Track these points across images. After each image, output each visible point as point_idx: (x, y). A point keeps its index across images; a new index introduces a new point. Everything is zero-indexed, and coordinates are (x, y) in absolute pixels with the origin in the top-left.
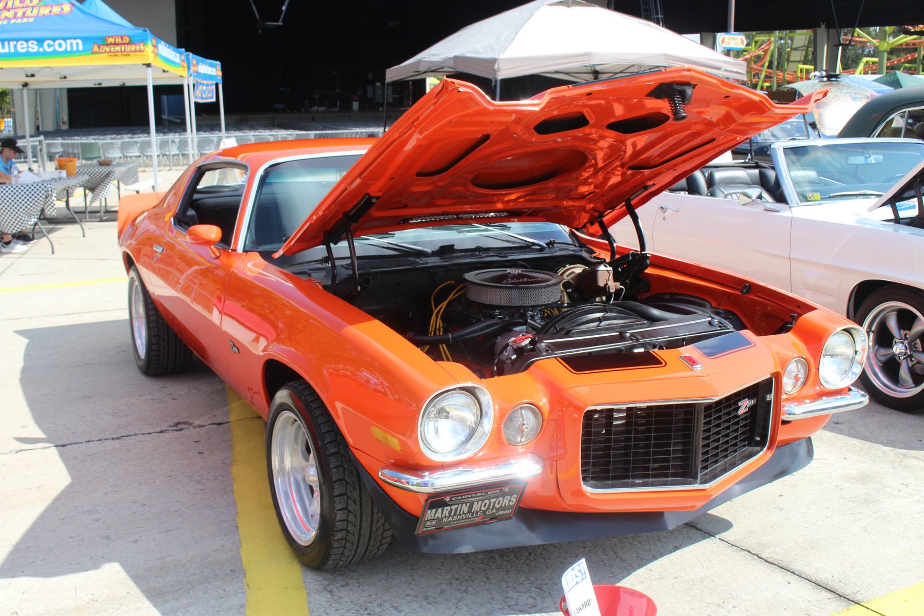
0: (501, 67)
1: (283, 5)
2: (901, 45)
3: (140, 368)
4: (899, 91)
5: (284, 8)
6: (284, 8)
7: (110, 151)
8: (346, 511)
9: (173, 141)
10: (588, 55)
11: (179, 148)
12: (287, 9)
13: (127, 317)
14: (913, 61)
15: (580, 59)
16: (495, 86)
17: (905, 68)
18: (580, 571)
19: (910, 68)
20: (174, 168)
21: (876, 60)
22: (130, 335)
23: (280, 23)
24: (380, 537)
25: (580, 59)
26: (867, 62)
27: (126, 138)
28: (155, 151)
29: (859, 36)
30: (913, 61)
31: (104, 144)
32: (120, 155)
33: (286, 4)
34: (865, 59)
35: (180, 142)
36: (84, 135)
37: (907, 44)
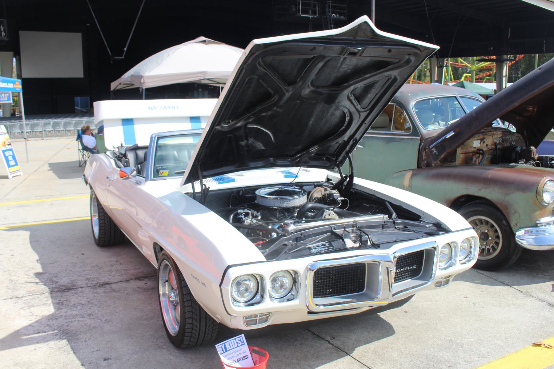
0: (146, 81)
1: (125, 47)
2: (482, 67)
3: (96, 243)
4: (223, 94)
5: (125, 49)
6: (125, 49)
7: (14, 129)
8: (191, 313)
9: (49, 123)
10: (204, 73)
11: (53, 127)
12: (127, 50)
13: (90, 218)
14: (490, 76)
15: (199, 75)
16: (142, 92)
17: (487, 79)
18: (240, 340)
19: (489, 79)
20: (45, 138)
21: (470, 75)
22: (91, 226)
23: (123, 58)
24: (212, 325)
25: (199, 75)
26: (466, 77)
27: (68, 120)
28: (27, 129)
29: (461, 63)
30: (490, 76)
31: (9, 125)
32: (19, 131)
33: (127, 47)
34: (465, 75)
35: (53, 124)
36: (34, 118)
37: (486, 67)
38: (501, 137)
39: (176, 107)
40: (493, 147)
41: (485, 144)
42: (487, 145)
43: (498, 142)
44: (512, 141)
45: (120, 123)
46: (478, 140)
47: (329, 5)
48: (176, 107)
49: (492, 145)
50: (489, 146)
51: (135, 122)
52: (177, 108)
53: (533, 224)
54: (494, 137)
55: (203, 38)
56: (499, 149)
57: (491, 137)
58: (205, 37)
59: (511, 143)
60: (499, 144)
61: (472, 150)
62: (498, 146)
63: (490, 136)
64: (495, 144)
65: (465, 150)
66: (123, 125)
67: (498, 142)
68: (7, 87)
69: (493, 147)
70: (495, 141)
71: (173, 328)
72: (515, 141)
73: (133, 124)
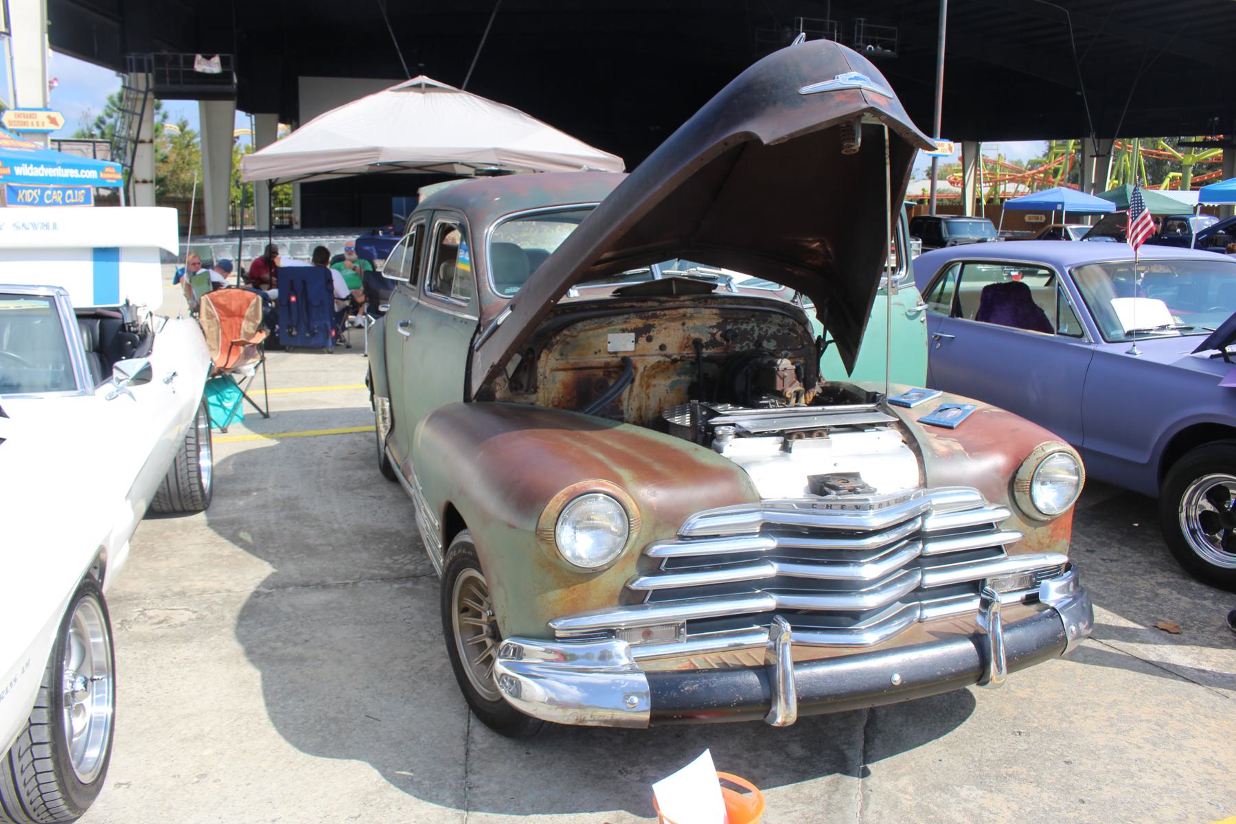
9: (284, 245)
10: (376, 150)
35: (292, 245)
38: (718, 326)
39: (51, 226)
40: (689, 352)
41: (655, 345)
42: (662, 347)
43: (705, 338)
44: (761, 338)
45: (90, 255)
46: (623, 331)
47: (859, 27)
48: (51, 226)
49: (683, 347)
50: (669, 351)
51: (123, 255)
52: (55, 227)
53: (539, 629)
54: (690, 324)
55: (423, 79)
56: (710, 359)
57: (678, 325)
58: (430, 77)
59: (758, 344)
60: (713, 343)
61: (602, 359)
62: (706, 352)
63: (673, 320)
64: (697, 344)
65: (573, 359)
66: (95, 260)
67: (705, 338)
68: (77, 176)
69: (689, 352)
70: (694, 335)
71: (634, 586)
72: (774, 336)
73: (118, 260)
